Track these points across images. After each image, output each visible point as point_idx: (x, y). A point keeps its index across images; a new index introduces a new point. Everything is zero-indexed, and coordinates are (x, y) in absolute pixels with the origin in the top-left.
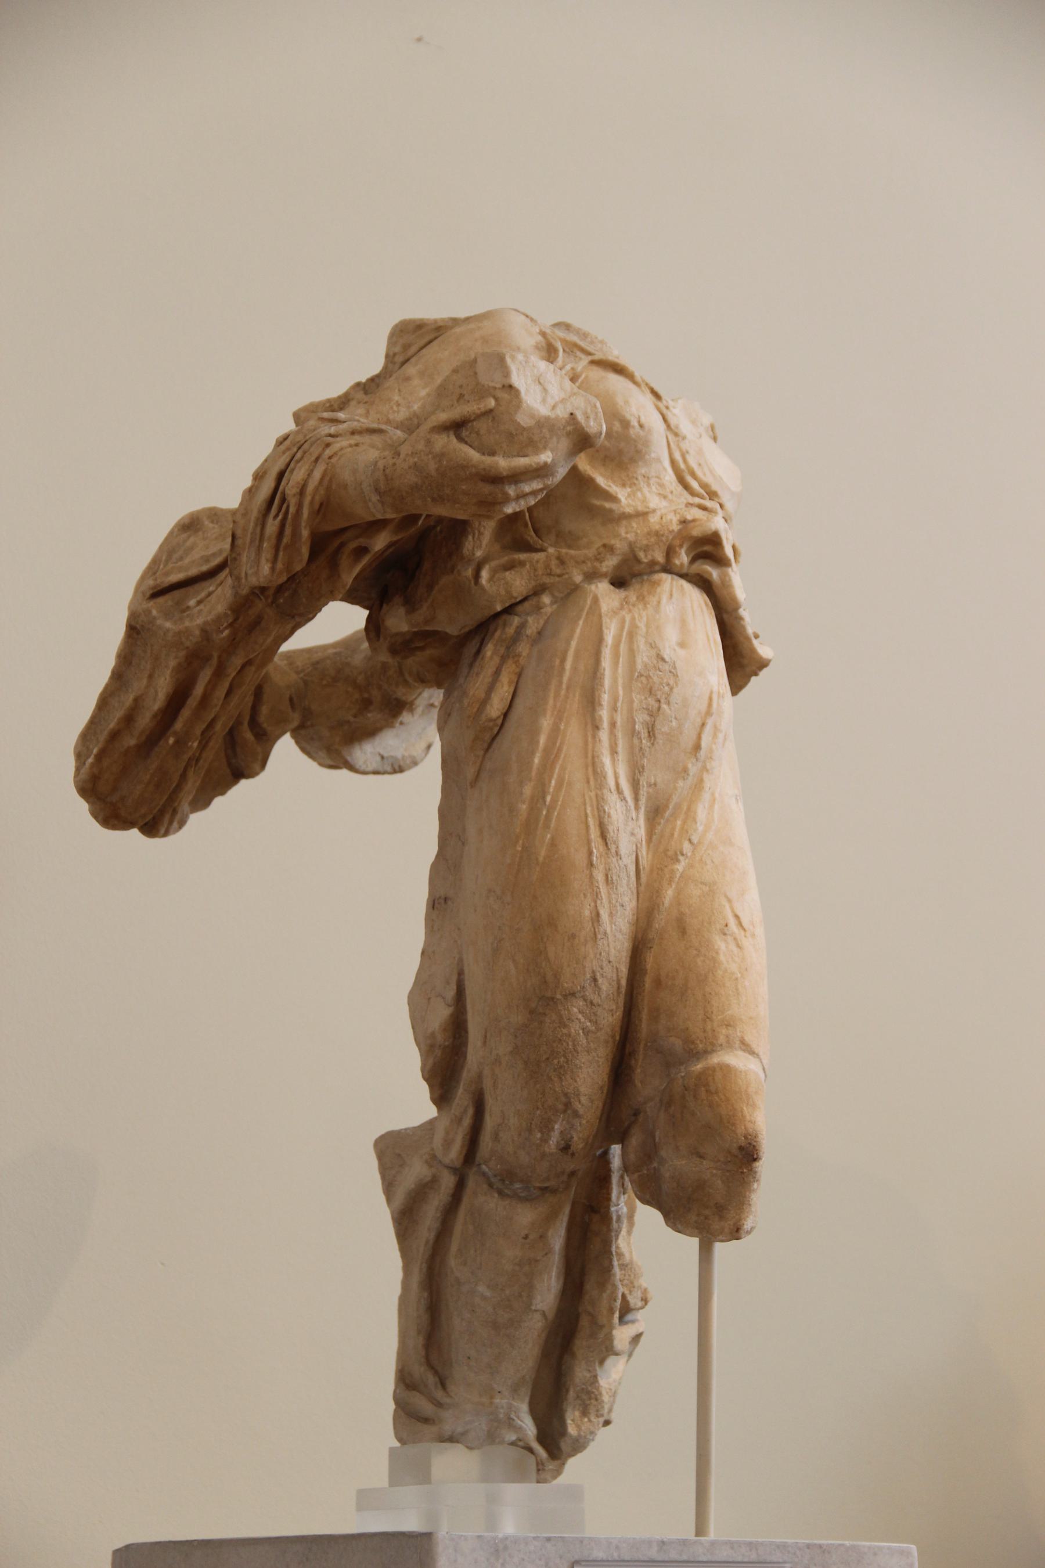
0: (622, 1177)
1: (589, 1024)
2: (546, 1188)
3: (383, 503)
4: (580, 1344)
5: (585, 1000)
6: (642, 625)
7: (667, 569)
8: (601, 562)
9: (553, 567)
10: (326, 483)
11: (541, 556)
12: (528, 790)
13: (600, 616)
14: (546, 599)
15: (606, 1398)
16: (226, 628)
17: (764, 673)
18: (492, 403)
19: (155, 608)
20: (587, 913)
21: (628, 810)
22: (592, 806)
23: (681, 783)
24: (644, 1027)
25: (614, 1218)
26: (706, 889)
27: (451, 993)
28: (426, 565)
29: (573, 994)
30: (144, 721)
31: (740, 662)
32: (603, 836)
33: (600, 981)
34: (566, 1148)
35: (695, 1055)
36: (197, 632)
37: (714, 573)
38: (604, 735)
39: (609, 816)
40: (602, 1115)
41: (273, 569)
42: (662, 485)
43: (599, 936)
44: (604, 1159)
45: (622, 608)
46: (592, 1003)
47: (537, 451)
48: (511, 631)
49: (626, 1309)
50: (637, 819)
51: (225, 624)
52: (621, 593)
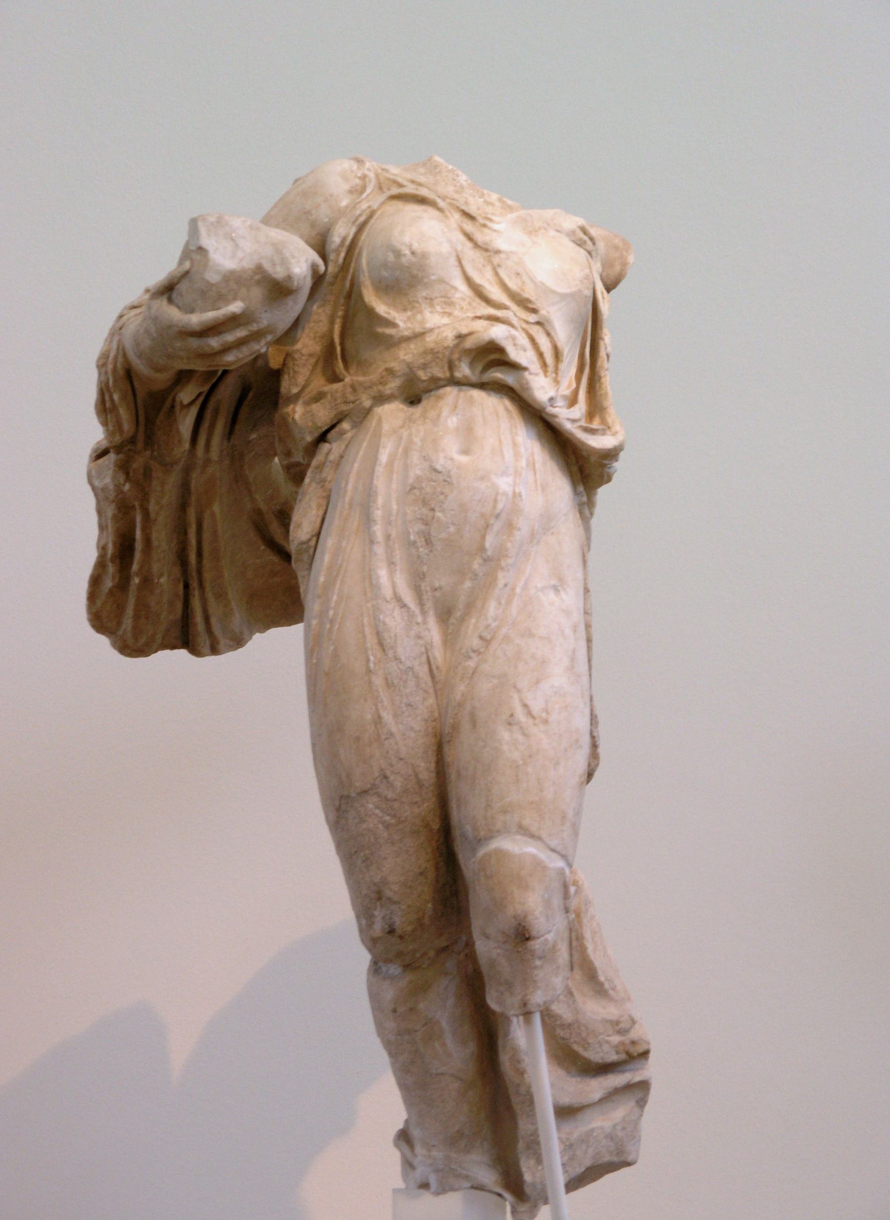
6: (417, 440)
9: (348, 395)
14: (345, 425)
26: (495, 681)
33: (392, 778)
34: (391, 932)
37: (508, 378)
38: (380, 550)
39: (384, 624)
43: (383, 737)
45: (402, 427)
47: (228, 302)
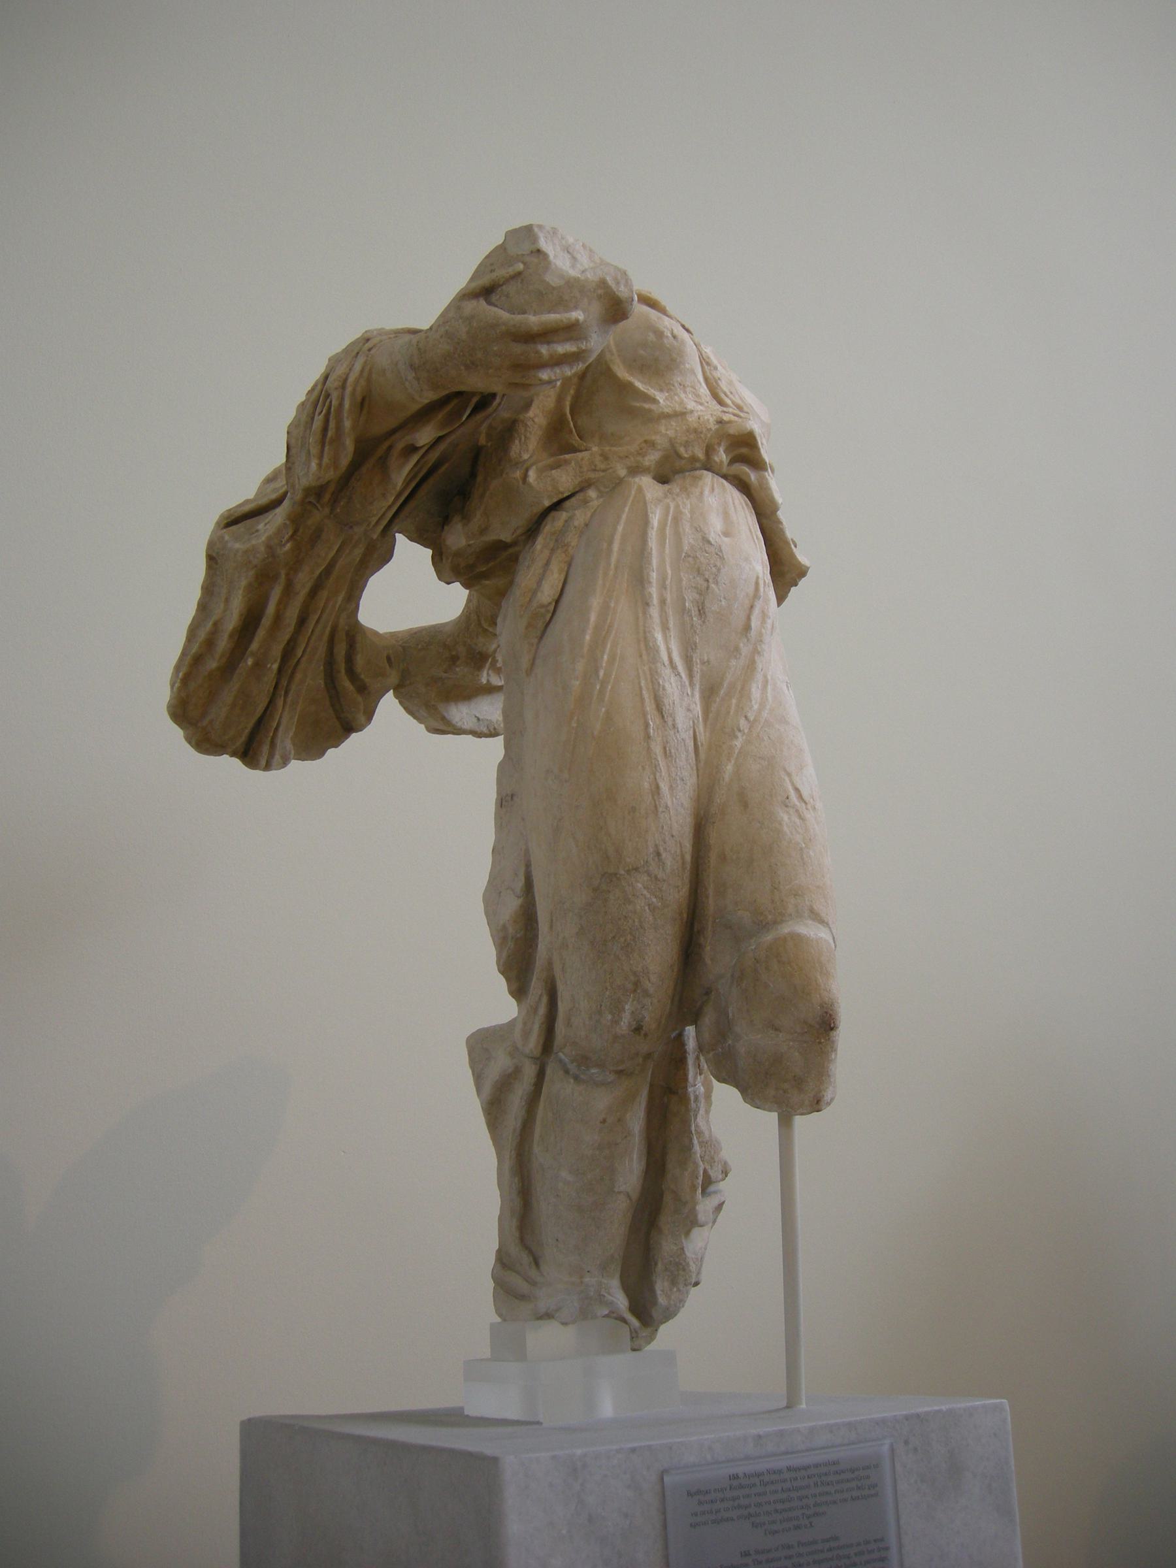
0: (698, 1058)
1: (654, 900)
2: (621, 1071)
3: (418, 379)
4: (665, 1220)
5: (649, 875)
7: (708, 466)
8: (644, 456)
10: (366, 374)
11: (586, 454)
12: (580, 666)
13: (645, 503)
14: (592, 493)
15: (693, 1267)
16: (288, 541)
17: (803, 582)
18: (521, 266)
19: (227, 535)
20: (646, 785)
21: (683, 686)
22: (646, 679)
23: (733, 662)
24: (711, 904)
25: (692, 1098)
27: (520, 883)
28: (480, 478)
29: (636, 869)
30: (223, 644)
31: (784, 571)
32: (659, 708)
33: (664, 855)
34: (638, 1029)
35: (763, 925)
36: (262, 549)
37: (753, 477)
38: (654, 612)
39: (664, 689)
40: (674, 996)
41: (320, 465)
42: (698, 396)
43: (660, 810)
44: (680, 1040)
45: (666, 497)
46: (656, 878)
48: (559, 523)
49: (708, 1181)
50: (693, 695)
51: (287, 537)
52: (666, 487)
